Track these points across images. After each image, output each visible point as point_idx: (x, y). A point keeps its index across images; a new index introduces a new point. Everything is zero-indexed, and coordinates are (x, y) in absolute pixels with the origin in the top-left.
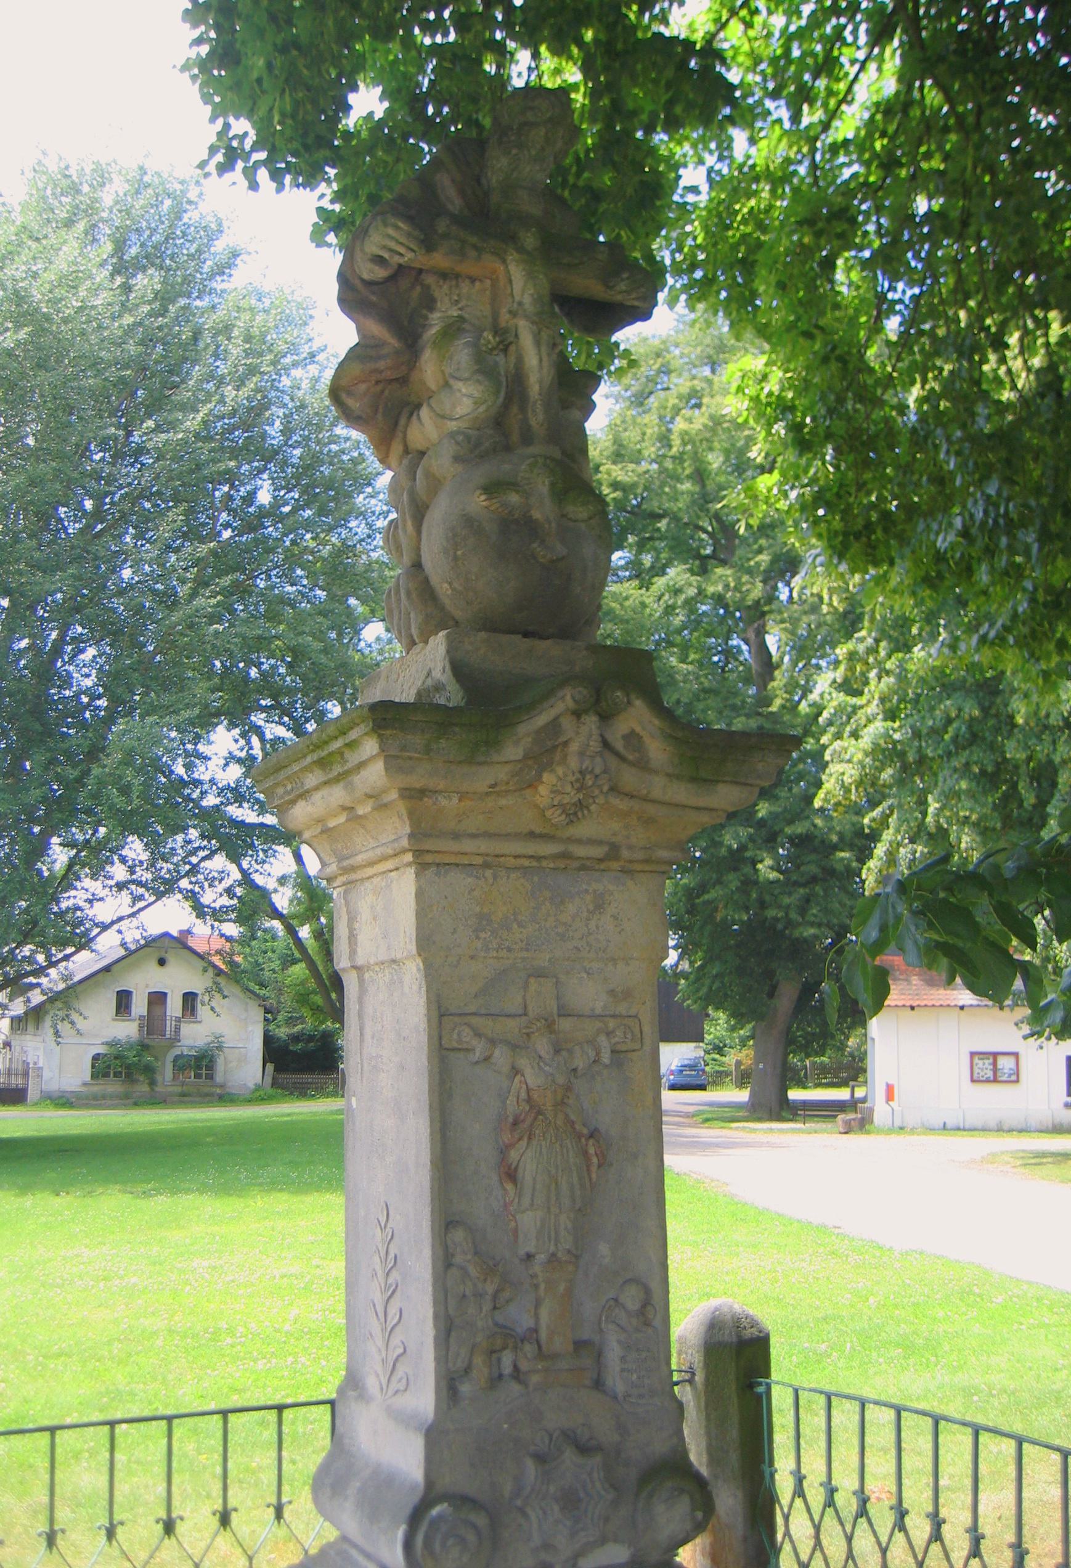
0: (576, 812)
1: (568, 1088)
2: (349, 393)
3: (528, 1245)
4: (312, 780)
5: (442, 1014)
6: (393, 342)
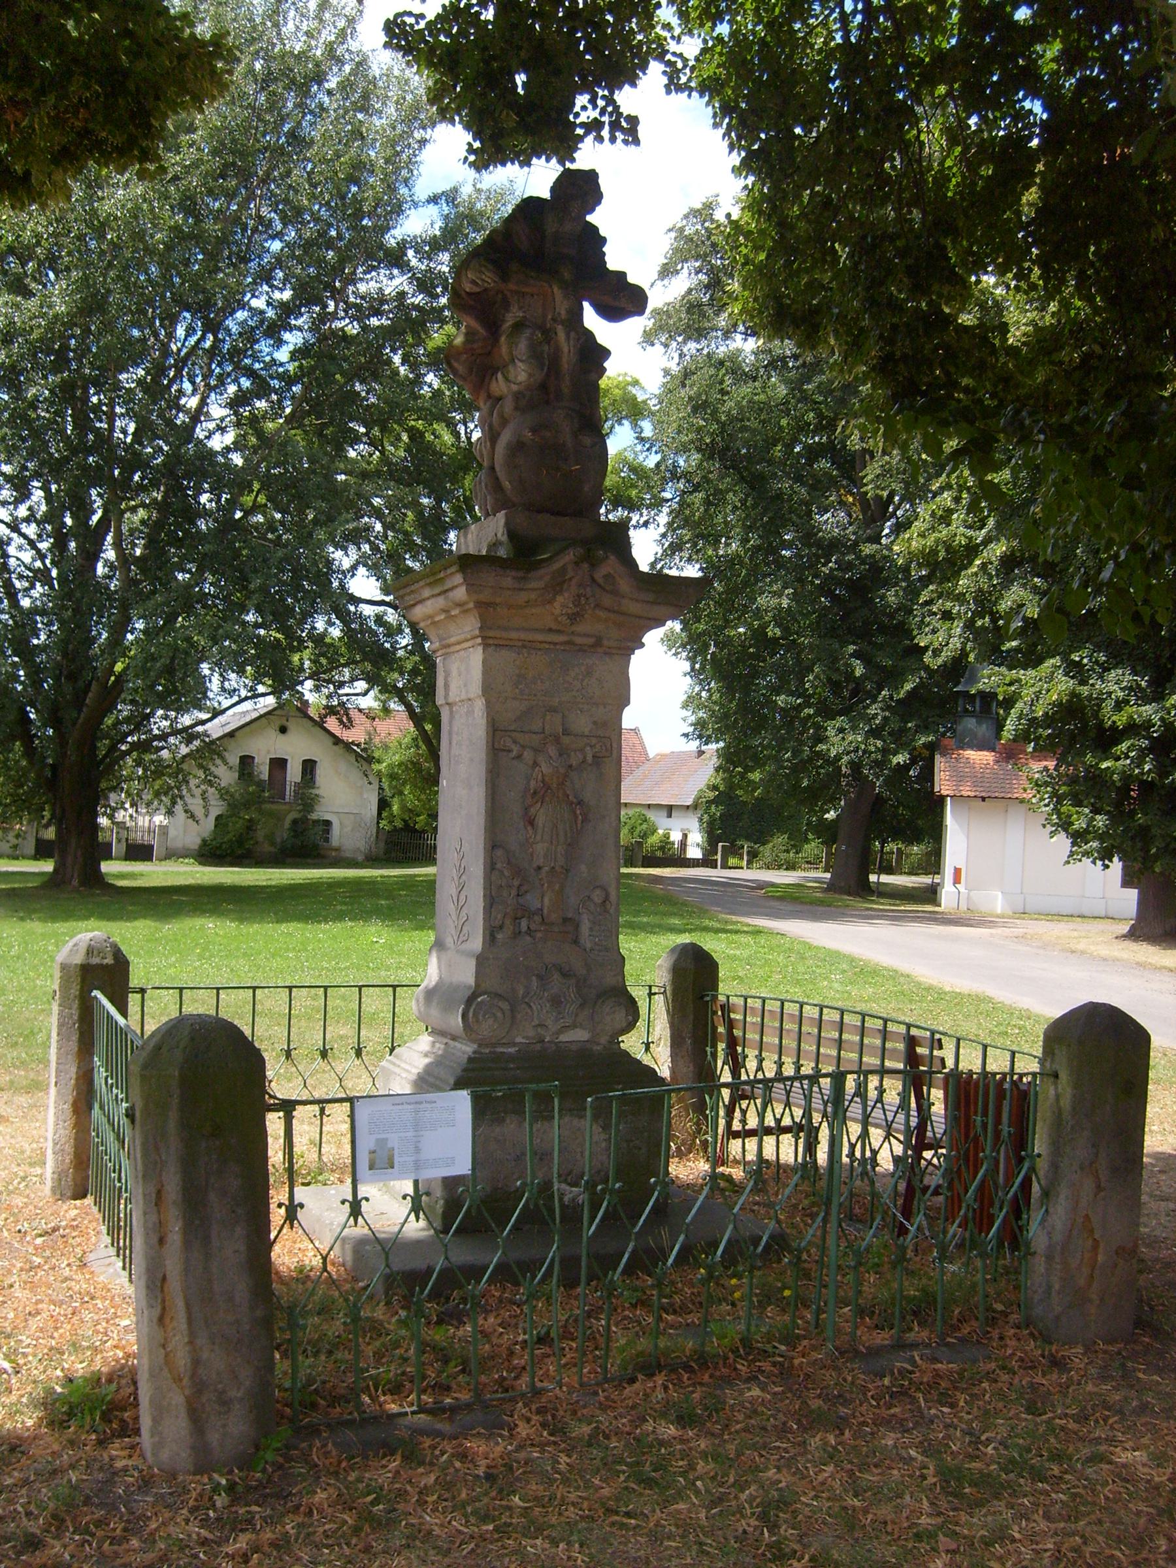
0: (574, 618)
1: (566, 776)
2: (457, 360)
3: (540, 861)
4: (427, 593)
5: (495, 729)
6: (482, 331)
